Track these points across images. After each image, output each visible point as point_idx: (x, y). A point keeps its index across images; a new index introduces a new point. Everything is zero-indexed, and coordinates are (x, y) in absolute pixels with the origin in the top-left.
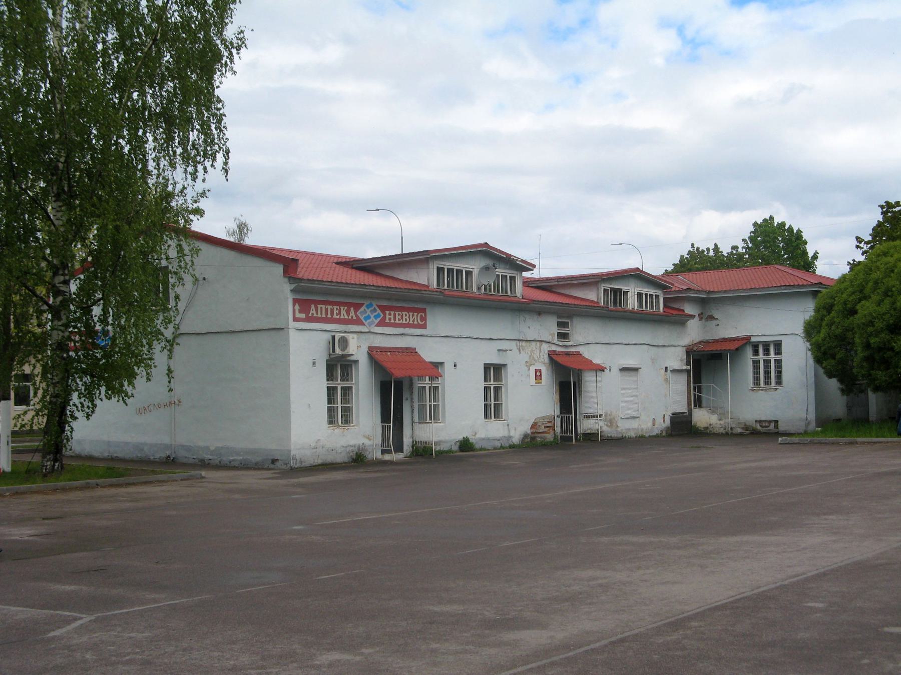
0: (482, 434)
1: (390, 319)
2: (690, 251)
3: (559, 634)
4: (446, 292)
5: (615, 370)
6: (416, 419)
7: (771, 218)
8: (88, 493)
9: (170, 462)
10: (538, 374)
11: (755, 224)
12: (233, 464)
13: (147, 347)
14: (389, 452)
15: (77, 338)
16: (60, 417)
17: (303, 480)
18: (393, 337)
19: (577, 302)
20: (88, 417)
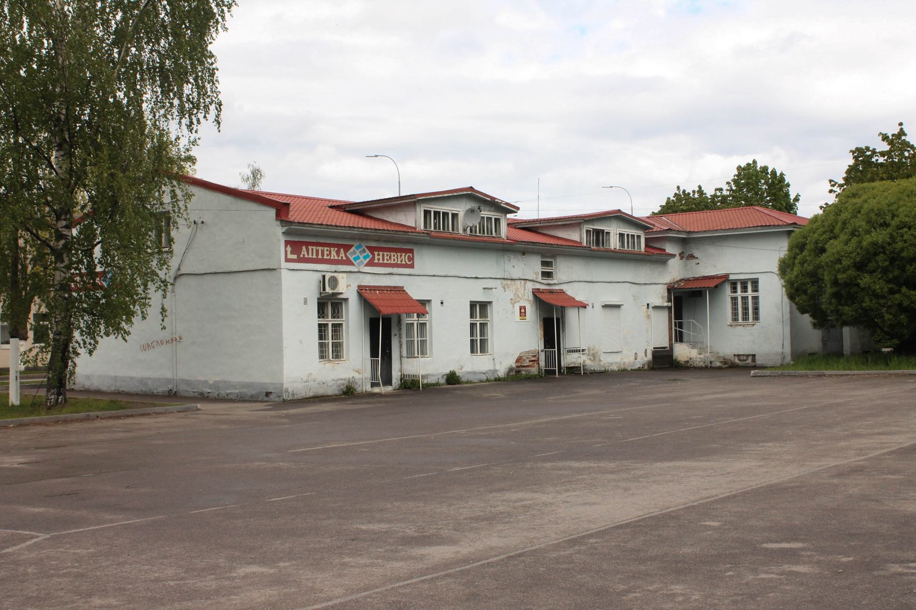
0: (468, 368)
1: (379, 259)
2: (676, 194)
3: (464, 549)
4: (433, 234)
5: (598, 307)
6: (404, 354)
7: (755, 162)
8: (86, 425)
9: (172, 395)
10: (523, 311)
11: (739, 168)
12: (230, 397)
13: (142, 287)
14: (377, 385)
15: (78, 279)
16: (63, 354)
17: (292, 411)
18: (381, 277)
19: (560, 242)
20: (91, 352)
